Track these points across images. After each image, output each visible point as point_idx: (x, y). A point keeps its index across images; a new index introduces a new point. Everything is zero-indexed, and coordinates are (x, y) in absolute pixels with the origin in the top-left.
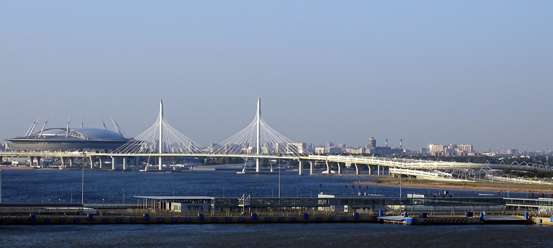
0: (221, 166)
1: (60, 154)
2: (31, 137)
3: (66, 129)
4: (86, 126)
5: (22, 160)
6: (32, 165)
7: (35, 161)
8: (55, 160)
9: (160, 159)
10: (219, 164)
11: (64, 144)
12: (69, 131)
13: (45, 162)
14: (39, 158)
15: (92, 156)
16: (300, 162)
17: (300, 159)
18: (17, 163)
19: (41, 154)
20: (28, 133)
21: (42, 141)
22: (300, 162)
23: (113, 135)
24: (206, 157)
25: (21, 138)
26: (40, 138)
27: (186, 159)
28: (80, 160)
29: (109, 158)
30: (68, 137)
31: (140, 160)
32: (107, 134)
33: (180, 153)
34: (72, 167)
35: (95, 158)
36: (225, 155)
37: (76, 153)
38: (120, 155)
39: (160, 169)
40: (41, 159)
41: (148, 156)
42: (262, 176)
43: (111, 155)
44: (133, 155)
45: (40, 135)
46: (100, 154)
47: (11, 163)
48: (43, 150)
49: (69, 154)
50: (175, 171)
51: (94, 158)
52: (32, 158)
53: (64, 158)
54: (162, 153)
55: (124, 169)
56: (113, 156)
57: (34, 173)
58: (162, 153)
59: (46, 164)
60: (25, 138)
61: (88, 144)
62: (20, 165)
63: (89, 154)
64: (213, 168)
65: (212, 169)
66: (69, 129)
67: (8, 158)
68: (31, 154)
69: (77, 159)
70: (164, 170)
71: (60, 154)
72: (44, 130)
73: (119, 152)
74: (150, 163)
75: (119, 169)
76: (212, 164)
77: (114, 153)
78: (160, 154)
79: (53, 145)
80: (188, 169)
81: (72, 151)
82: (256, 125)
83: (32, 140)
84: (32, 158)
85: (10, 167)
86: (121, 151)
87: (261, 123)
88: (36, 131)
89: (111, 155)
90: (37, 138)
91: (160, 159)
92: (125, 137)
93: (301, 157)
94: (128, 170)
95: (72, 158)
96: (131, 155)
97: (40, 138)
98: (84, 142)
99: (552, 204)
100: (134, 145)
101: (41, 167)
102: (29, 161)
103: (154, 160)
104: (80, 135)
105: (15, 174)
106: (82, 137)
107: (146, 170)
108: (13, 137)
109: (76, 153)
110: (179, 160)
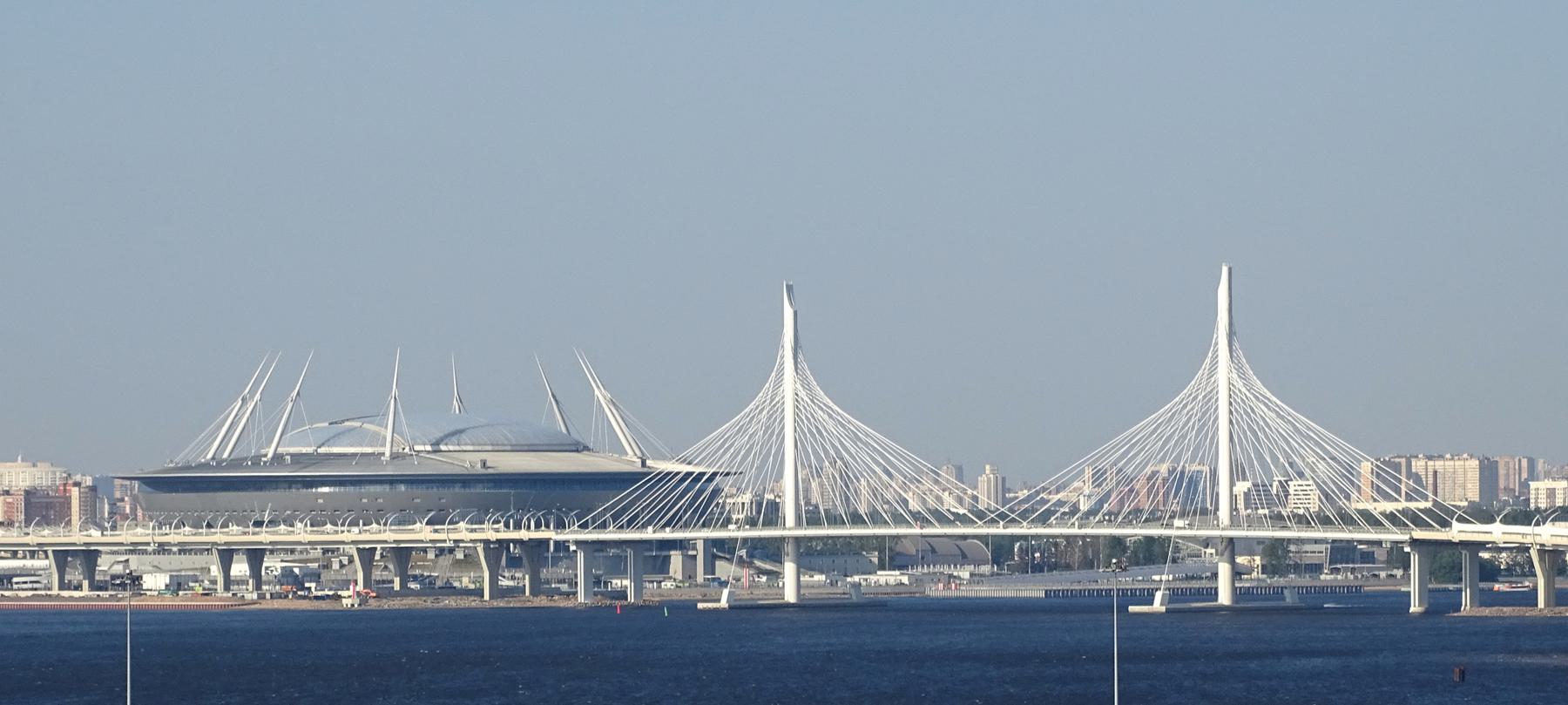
7: (240, 568)
13: (287, 574)
14: (256, 556)
17: (1414, 543)
24: (1014, 538)
27: (764, 548)
30: (394, 456)
36: (1075, 531)
40: (268, 562)
52: (227, 556)
56: (577, 543)
61: (478, 490)
65: (1032, 589)
67: (133, 558)
73: (604, 526)
75: (1442, 605)
76: (1037, 568)
77: (584, 526)
82: (1211, 398)
86: (615, 517)
89: (571, 535)
93: (1419, 534)
99: (1567, 514)
102: (215, 571)
107: (724, 603)
108: (154, 467)
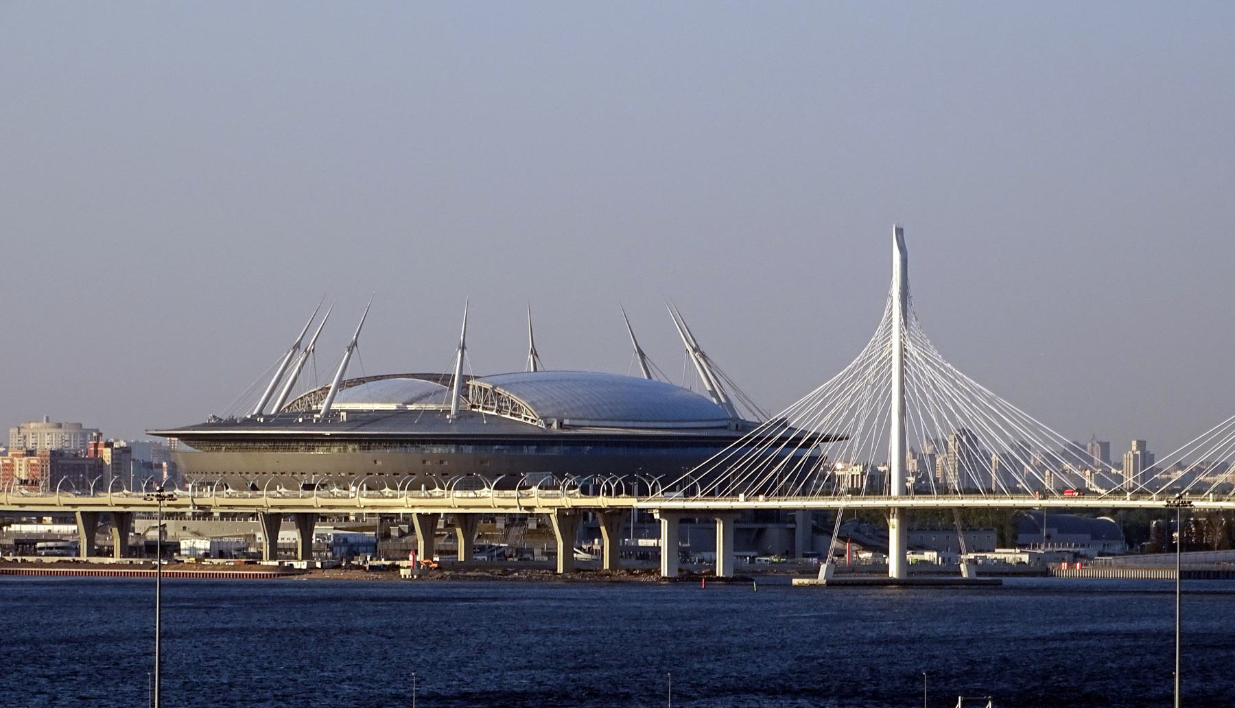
0: (1211, 555)
1: (405, 503)
2: (283, 418)
3: (447, 379)
4: (553, 363)
5: (232, 533)
6: (273, 557)
7: (289, 535)
8: (394, 532)
9: (894, 522)
10: (1208, 547)
11: (437, 450)
12: (464, 390)
13: (340, 542)
14: (305, 522)
15: (561, 512)
16: (664, 524)
18: (203, 545)
19: (315, 502)
20: (261, 399)
21: (332, 440)
22: (664, 524)
23: (693, 406)
25: (232, 423)
26: (322, 423)
28: (514, 531)
29: (646, 522)
30: (462, 415)
31: (816, 530)
32: (653, 400)
33: (1015, 491)
34: (468, 565)
35: (579, 524)
37: (489, 499)
38: (698, 503)
39: (893, 572)
40: (319, 528)
41: (836, 510)
42: (911, 595)
43: (654, 503)
44: (773, 504)
45: (323, 407)
46: (602, 501)
47: (176, 547)
48: (272, 487)
49: (451, 501)
50: (967, 583)
51: (570, 518)
53: (429, 521)
54: (905, 492)
55: (720, 572)
56: (664, 512)
57: (279, 595)
58: (905, 492)
59: (347, 550)
60: (251, 422)
61: (555, 451)
62: (221, 555)
63: (545, 500)
64: (1169, 566)
66: (464, 378)
67: (171, 524)
68: (266, 501)
69: (500, 525)
70: (914, 578)
71: (405, 503)
72: (342, 385)
74: (968, 551)
78: (894, 500)
79: (383, 457)
80: (1047, 573)
81: (470, 484)
82: (886, 364)
83: (283, 435)
84: (273, 522)
85: (163, 568)
86: (703, 483)
87: (910, 346)
88: (302, 392)
89: (654, 503)
90: (307, 423)
91: (894, 522)
92: (745, 415)
94: (739, 578)
95: (467, 521)
96: (752, 504)
97: (322, 423)
98: (541, 441)
100: (800, 460)
101: (311, 567)
103: (868, 529)
104: (516, 410)
105: (201, 595)
106: (529, 419)
107: (821, 578)
108: (194, 417)
109: (489, 499)
110: (1013, 527)
